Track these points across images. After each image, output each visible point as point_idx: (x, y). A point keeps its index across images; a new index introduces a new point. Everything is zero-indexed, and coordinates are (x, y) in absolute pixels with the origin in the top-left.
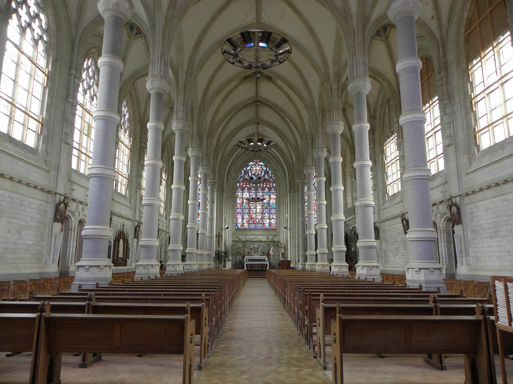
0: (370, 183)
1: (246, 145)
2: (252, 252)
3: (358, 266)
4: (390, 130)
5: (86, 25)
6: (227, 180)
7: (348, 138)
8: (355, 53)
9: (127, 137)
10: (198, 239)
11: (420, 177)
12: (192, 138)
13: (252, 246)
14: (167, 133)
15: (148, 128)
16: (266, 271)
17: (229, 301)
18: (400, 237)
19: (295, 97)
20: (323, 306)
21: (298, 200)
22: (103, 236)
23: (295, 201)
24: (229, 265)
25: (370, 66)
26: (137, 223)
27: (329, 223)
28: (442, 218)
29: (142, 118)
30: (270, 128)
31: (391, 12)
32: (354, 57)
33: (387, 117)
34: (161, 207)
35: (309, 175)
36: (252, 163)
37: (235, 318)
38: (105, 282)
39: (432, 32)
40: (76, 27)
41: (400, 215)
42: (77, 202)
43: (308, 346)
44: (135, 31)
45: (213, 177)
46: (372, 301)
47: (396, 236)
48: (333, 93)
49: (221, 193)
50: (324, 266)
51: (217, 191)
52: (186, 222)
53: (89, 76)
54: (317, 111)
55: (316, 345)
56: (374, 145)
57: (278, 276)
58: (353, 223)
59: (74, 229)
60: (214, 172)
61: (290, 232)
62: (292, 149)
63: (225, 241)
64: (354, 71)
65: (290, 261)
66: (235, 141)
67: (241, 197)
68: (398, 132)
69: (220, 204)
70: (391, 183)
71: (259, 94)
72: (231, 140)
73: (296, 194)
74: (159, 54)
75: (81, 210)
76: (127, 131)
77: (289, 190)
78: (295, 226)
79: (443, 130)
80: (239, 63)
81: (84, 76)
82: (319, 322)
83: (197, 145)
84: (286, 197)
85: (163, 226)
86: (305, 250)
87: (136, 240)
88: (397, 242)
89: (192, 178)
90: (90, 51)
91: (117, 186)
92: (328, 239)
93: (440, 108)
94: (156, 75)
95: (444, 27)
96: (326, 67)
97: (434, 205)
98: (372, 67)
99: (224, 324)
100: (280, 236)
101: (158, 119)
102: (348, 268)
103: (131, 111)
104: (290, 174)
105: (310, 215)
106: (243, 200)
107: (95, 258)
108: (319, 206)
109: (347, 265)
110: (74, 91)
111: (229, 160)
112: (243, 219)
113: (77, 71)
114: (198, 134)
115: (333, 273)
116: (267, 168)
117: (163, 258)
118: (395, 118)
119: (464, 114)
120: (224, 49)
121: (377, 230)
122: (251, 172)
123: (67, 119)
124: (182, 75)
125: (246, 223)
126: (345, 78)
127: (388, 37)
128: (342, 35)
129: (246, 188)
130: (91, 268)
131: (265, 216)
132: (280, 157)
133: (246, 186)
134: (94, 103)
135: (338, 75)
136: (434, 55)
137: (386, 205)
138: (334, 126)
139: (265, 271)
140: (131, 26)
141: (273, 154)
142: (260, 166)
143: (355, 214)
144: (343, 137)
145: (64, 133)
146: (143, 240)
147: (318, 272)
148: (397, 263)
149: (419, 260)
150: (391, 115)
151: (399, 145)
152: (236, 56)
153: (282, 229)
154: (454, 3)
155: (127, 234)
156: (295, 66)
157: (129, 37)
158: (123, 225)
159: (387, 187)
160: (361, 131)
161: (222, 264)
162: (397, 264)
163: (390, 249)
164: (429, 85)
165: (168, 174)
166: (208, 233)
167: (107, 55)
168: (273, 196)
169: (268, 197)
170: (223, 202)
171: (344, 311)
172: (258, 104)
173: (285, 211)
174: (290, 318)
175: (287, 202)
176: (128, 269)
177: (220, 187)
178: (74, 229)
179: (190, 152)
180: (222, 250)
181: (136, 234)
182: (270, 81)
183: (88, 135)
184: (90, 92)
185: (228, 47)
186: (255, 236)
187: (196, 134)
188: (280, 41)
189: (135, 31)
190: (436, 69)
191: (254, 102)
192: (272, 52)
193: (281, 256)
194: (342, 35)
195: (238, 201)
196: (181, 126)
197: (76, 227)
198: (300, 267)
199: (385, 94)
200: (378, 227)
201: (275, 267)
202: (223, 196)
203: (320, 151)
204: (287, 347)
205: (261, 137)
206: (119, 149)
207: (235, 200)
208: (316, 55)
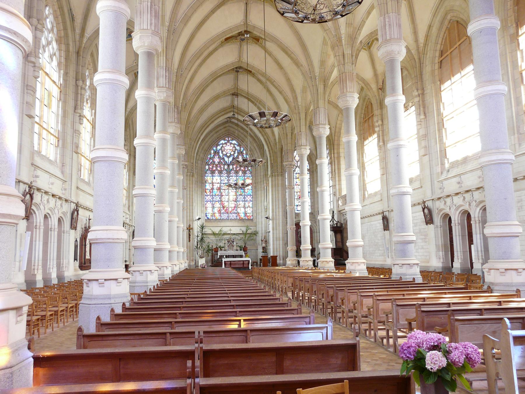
3: (348, 263)
15: (136, 97)
23: (278, 186)
28: (477, 206)
32: (386, 15)
45: (184, 158)
46: (184, 302)
49: (191, 178)
56: (382, 121)
59: (40, 226)
67: (211, 182)
71: (242, 59)
74: (148, 2)
83: (174, 119)
85: (127, 218)
94: (145, 29)
100: (258, 226)
102: (334, 263)
111: (199, 138)
112: (213, 207)
113: (38, 20)
117: (128, 257)
118: (416, 91)
119: (511, 87)
122: (222, 153)
123: (29, 84)
131: (240, 204)
133: (217, 169)
138: (348, 99)
145: (25, 103)
151: (420, 123)
158: (89, 220)
173: (263, 199)
177: (189, 171)
178: (40, 226)
182: (256, 44)
183: (49, 106)
184: (49, 50)
186: (228, 228)
187: (173, 106)
196: (163, 96)
197: (42, 224)
203: (323, 129)
207: (204, 185)
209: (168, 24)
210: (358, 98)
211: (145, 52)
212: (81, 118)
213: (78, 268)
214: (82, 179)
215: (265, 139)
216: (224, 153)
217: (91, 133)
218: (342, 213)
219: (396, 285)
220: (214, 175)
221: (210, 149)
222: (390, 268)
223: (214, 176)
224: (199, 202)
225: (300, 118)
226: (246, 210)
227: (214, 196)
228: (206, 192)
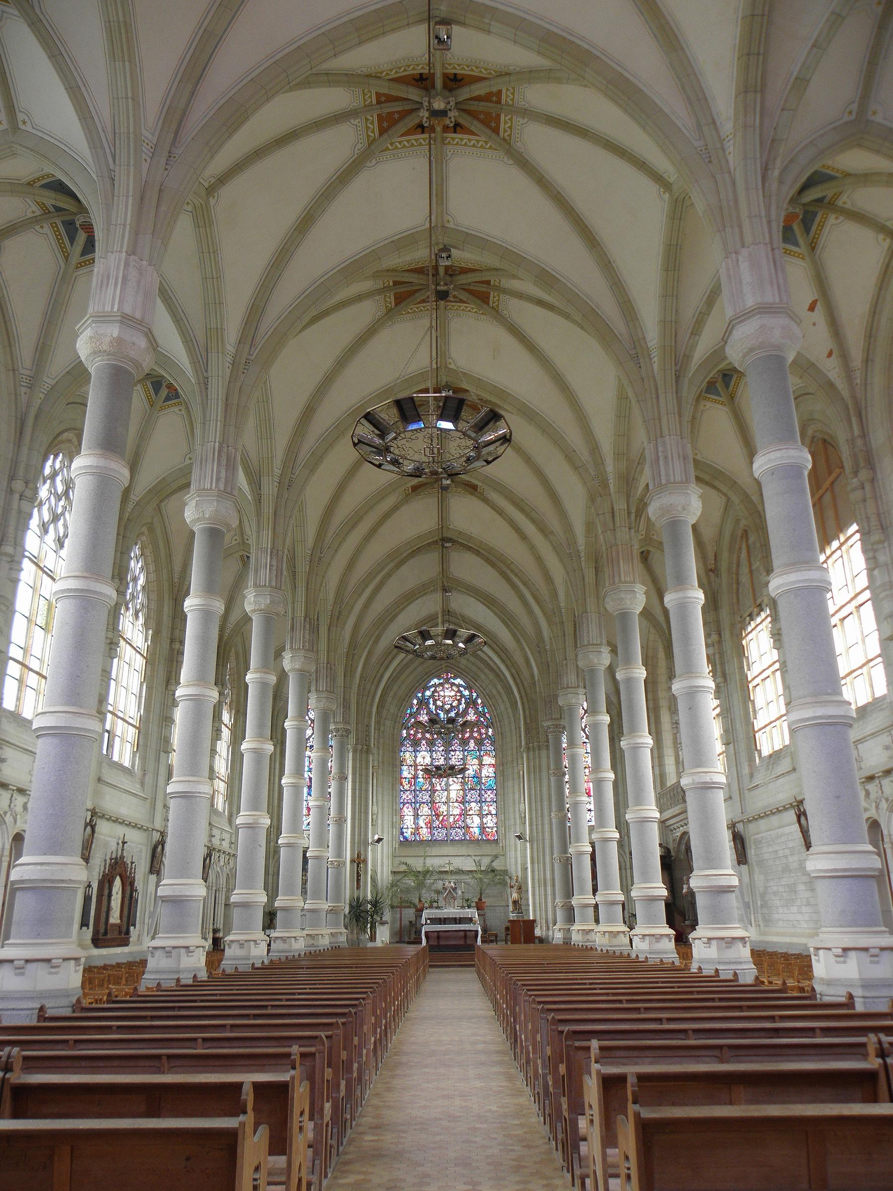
0: (715, 729)
1: (418, 646)
2: (441, 899)
3: (695, 939)
4: (755, 601)
5: (53, 382)
6: (378, 723)
7: (659, 619)
8: (661, 433)
9: (141, 629)
10: (305, 869)
11: (828, 719)
12: (292, 628)
13: (439, 885)
14: (234, 617)
15: (186, 610)
16: (474, 947)
17: (394, 1011)
18: (796, 858)
19: (530, 529)
20: (598, 1072)
21: (549, 768)
22: (63, 881)
23: (540, 772)
24: (383, 935)
25: (699, 457)
26: (156, 836)
27: (621, 825)
29: (177, 584)
30: (475, 598)
31: (733, 346)
33: (745, 570)
34: (218, 792)
35: (571, 709)
36: (435, 681)
37: (389, 1090)
38: (65, 1002)
39: (831, 385)
40: (31, 387)
41: (791, 804)
42: (11, 789)
43: (569, 1176)
44: (164, 392)
45: (343, 717)
46: (725, 1050)
47: (786, 857)
48: (617, 519)
49: (364, 755)
50: (614, 934)
51: (355, 751)
52: (275, 830)
53: (56, 494)
54: (583, 559)
55: (588, 1176)
56: (720, 635)
57: (500, 969)
58: (681, 823)
60: (346, 706)
61: (532, 848)
62: (529, 647)
63: (374, 872)
64: (660, 472)
65: (534, 921)
66: (391, 635)
67: (412, 763)
68: (772, 607)
69: (361, 783)
70: (766, 726)
71: (448, 523)
72: (385, 628)
73: (544, 753)
74: (215, 442)
75: (19, 809)
76: (140, 614)
77: (527, 744)
78: (543, 832)
79: (875, 600)
80: (393, 465)
81: (44, 492)
82: (592, 1115)
83: (303, 643)
84: (520, 761)
85: (223, 840)
86: (569, 893)
87: (153, 878)
88: (790, 871)
89: (292, 723)
90: (60, 438)
91: (110, 746)
92: (622, 860)
93: (865, 551)
94: (207, 490)
95: (858, 374)
96: (599, 462)
97: (871, 778)
98: (703, 460)
99: (360, 1109)
101: (209, 588)
102: (673, 940)
103: (152, 568)
104: (526, 704)
105: (576, 805)
106: (416, 770)
107: (42, 938)
108: (599, 783)
109: (672, 932)
110: (17, 529)
111: (382, 676)
112: (416, 816)
113: (27, 483)
114: (308, 619)
115: (637, 956)
116: (471, 692)
118: (764, 574)
120: (359, 435)
121: (739, 840)
122: (435, 703)
124: (269, 488)
125: (424, 826)
126: (642, 486)
127: (735, 394)
128: (631, 394)
129: (424, 742)
130: (30, 966)
132: (503, 668)
133: (424, 738)
134: (64, 553)
135: (628, 480)
136: (841, 436)
137: (757, 781)
138: (623, 595)
139: (471, 947)
140: (156, 383)
141: (487, 659)
142: (454, 688)
143: (685, 801)
144: (647, 618)
146: (169, 885)
147: (602, 950)
148: (795, 923)
149: (841, 926)
150: (754, 567)
152: (385, 450)
153: (512, 839)
154: (873, 321)
155: (132, 863)
156: (528, 460)
157: (152, 406)
158: (124, 843)
159: (757, 735)
160: (684, 607)
161: (365, 932)
162: (794, 926)
163: (775, 888)
164: (834, 498)
165: (237, 712)
166: (330, 854)
167: (94, 452)
168: (488, 760)
169: (476, 761)
170: (367, 776)
171: (654, 1084)
172: (447, 545)
173: (517, 796)
174: (529, 1088)
175: (521, 772)
176: (131, 953)
179: (288, 662)
180: (365, 896)
181: (155, 867)
182: (472, 494)
184: (56, 529)
185: (366, 431)
186: (447, 860)
188: (485, 415)
189: (164, 392)
190: (848, 465)
191: (436, 542)
192: (467, 440)
193: (511, 908)
194: (631, 394)
195: (405, 774)
196: (265, 602)
198: (558, 936)
199: (737, 520)
200: (742, 833)
201: (496, 936)
202: (367, 762)
203: (595, 653)
204: (517, 1179)
205: (451, 627)
206: (120, 657)
208: (574, 437)
209: (280, 472)
210: (645, 593)
211: (205, 529)
212: (113, 647)
213: (89, 942)
214: (116, 763)
215: (512, 675)
216: (439, 703)
217: (143, 672)
218: (668, 826)
219: (663, 982)
220: (418, 749)
221: (410, 697)
222: (805, 953)
223: (418, 751)
224: (386, 805)
225: (564, 632)
226: (485, 821)
227: (418, 793)
228: (401, 784)
